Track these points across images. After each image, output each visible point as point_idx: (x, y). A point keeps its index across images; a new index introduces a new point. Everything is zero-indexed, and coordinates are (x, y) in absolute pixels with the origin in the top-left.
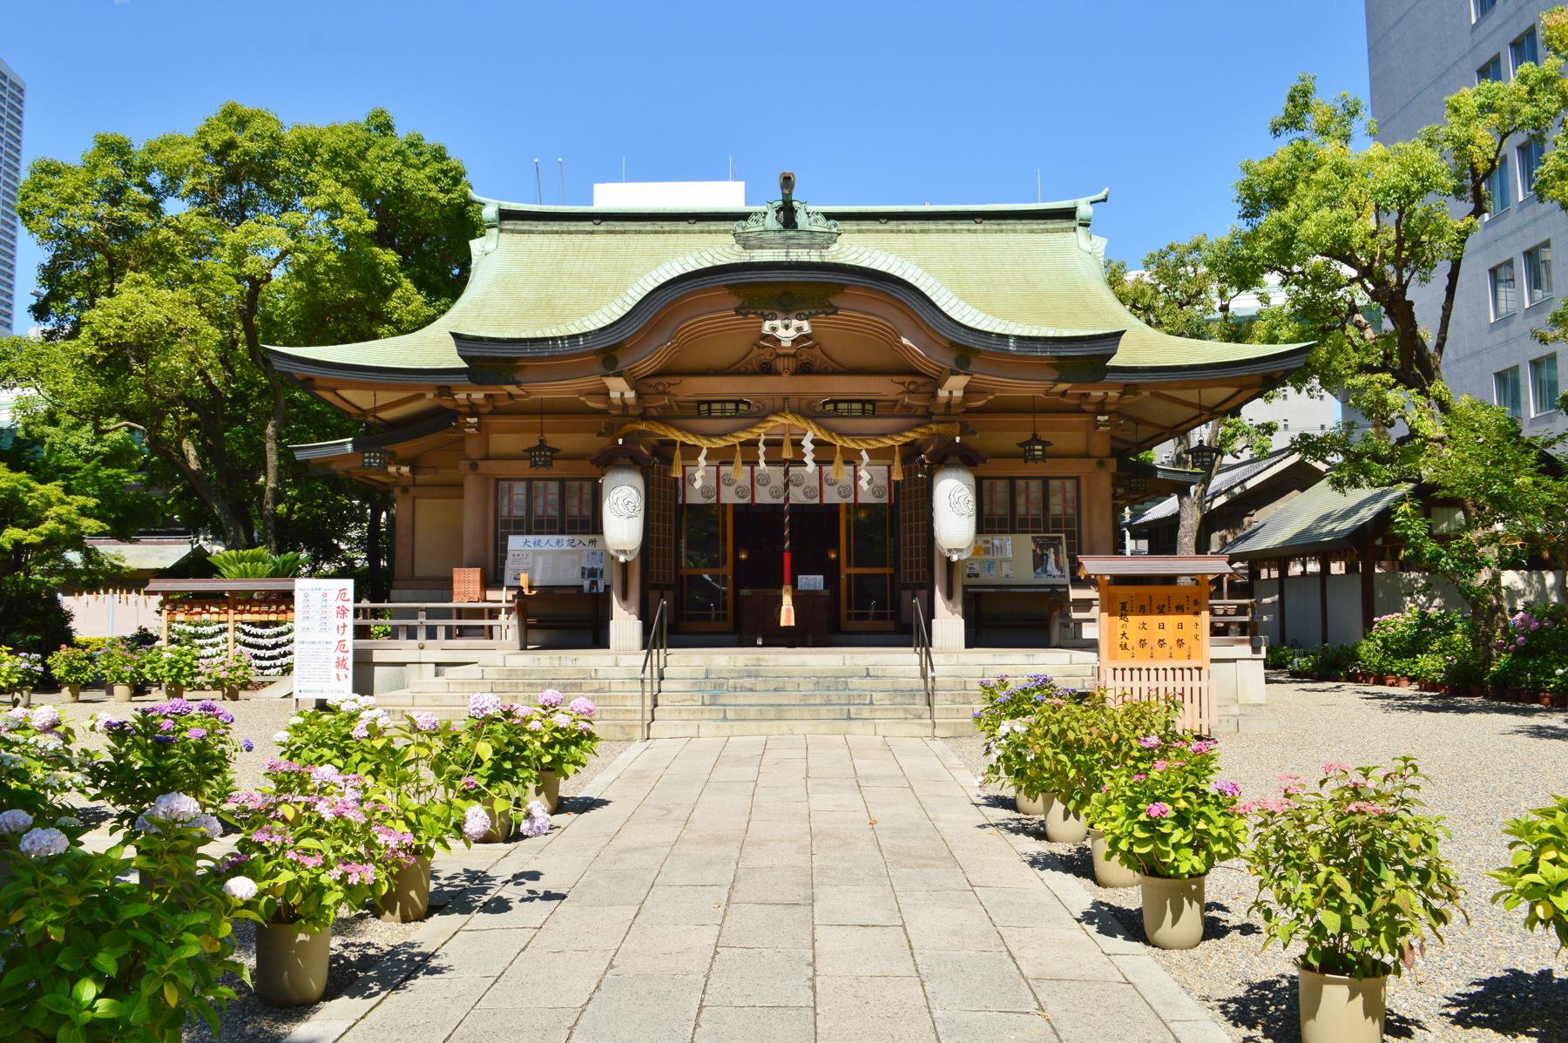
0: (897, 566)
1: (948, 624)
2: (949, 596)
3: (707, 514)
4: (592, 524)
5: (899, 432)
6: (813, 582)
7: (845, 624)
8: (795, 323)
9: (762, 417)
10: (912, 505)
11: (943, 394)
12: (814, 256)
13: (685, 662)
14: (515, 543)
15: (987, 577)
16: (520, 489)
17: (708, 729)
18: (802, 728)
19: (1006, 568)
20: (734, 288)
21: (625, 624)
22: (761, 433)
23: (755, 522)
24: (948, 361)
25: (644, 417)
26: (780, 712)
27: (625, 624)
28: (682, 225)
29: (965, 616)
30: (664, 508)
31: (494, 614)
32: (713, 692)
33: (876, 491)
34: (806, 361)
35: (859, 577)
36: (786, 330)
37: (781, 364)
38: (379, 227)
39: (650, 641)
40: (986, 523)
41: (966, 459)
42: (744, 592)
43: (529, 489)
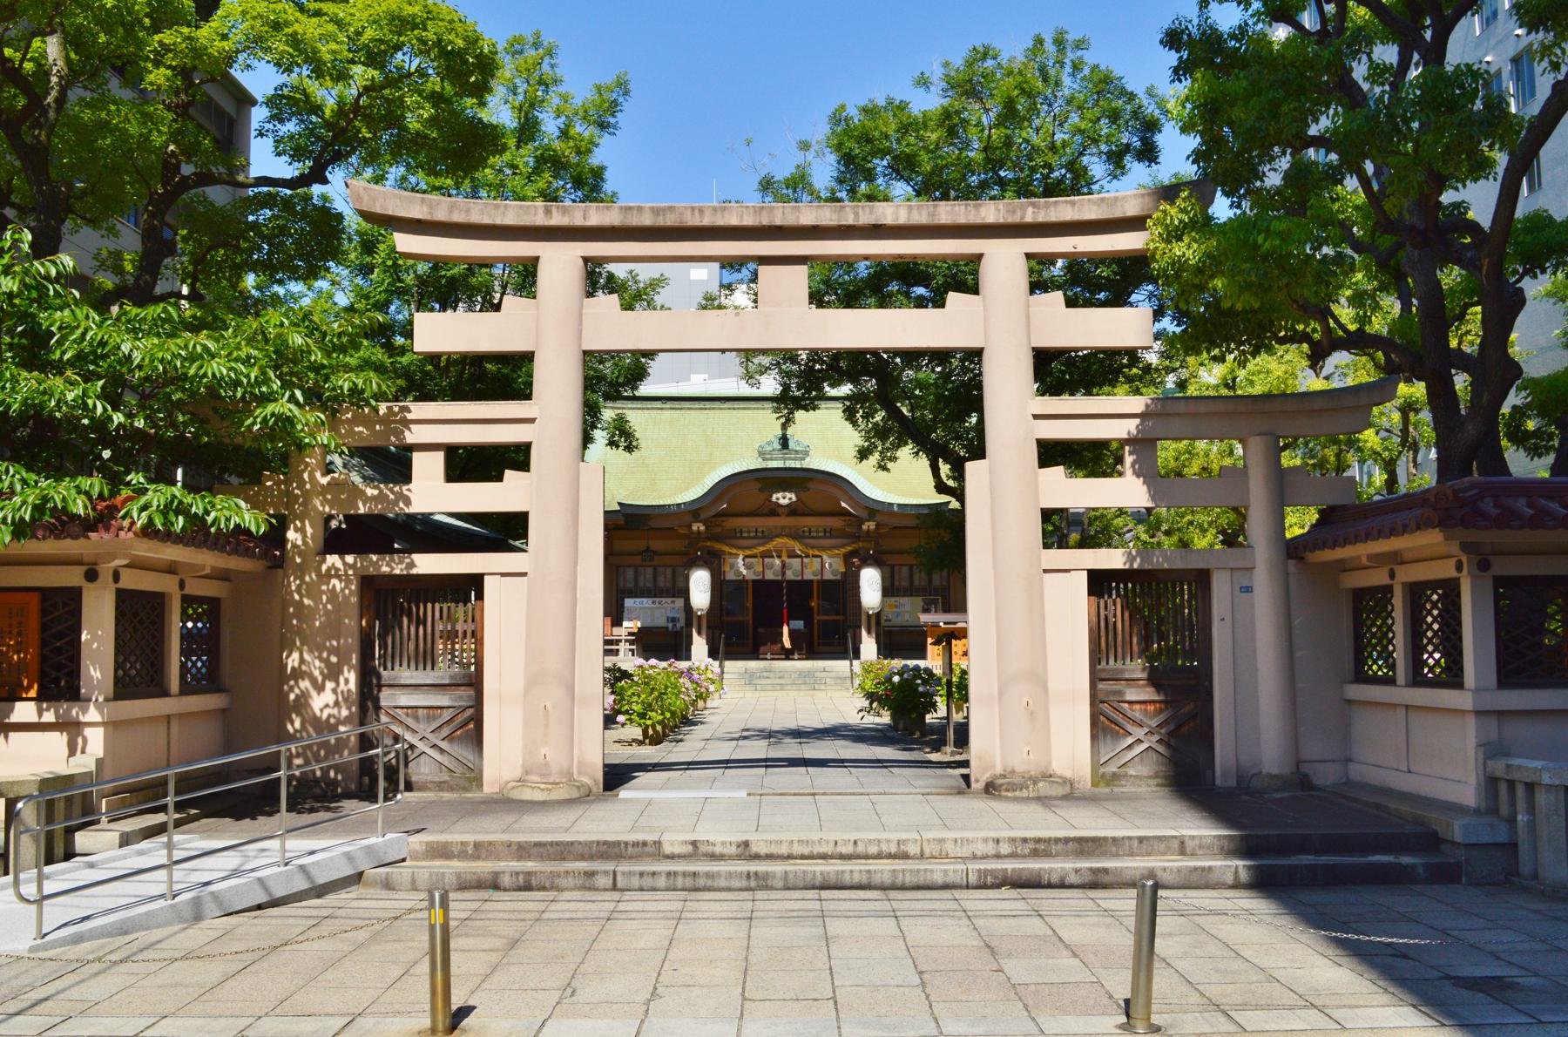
0: (844, 614)
1: (869, 647)
2: (869, 632)
3: (741, 584)
4: (685, 593)
5: (843, 546)
6: (799, 624)
7: (34, 602)
8: (788, 495)
9: (771, 538)
10: (850, 584)
11: (865, 527)
12: (797, 465)
13: (733, 667)
14: (629, 602)
15: (897, 621)
16: (630, 573)
17: (748, 694)
18: (792, 694)
19: (907, 617)
20: (757, 480)
21: (699, 646)
22: (770, 546)
23: (764, 590)
24: (864, 514)
25: (708, 539)
26: (782, 687)
27: (699, 646)
28: (717, 405)
29: (878, 642)
30: (719, 587)
31: (618, 642)
32: (750, 679)
33: (834, 573)
34: (792, 510)
35: (825, 622)
36: (784, 498)
37: (780, 511)
38: (700, 566)
39: (713, 654)
40: (888, 590)
41: (877, 562)
42: (761, 630)
43: (636, 572)
